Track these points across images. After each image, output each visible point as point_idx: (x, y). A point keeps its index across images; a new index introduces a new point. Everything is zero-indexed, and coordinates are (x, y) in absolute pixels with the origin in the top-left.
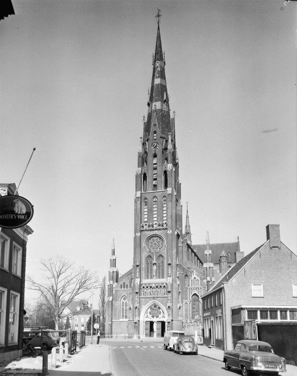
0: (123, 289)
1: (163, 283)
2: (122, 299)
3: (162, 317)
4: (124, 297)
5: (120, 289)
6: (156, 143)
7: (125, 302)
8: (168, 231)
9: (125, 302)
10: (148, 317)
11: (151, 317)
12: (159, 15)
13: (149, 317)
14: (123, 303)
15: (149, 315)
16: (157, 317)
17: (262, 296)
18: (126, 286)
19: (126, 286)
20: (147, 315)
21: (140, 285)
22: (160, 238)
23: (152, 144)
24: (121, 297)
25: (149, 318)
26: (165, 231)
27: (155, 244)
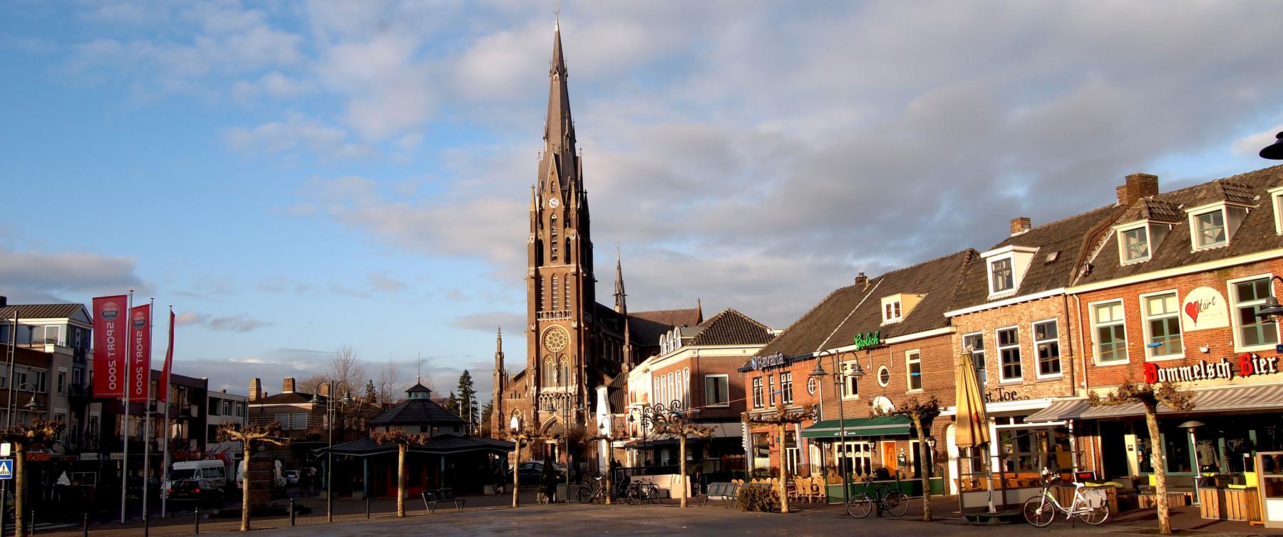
27: (556, 340)
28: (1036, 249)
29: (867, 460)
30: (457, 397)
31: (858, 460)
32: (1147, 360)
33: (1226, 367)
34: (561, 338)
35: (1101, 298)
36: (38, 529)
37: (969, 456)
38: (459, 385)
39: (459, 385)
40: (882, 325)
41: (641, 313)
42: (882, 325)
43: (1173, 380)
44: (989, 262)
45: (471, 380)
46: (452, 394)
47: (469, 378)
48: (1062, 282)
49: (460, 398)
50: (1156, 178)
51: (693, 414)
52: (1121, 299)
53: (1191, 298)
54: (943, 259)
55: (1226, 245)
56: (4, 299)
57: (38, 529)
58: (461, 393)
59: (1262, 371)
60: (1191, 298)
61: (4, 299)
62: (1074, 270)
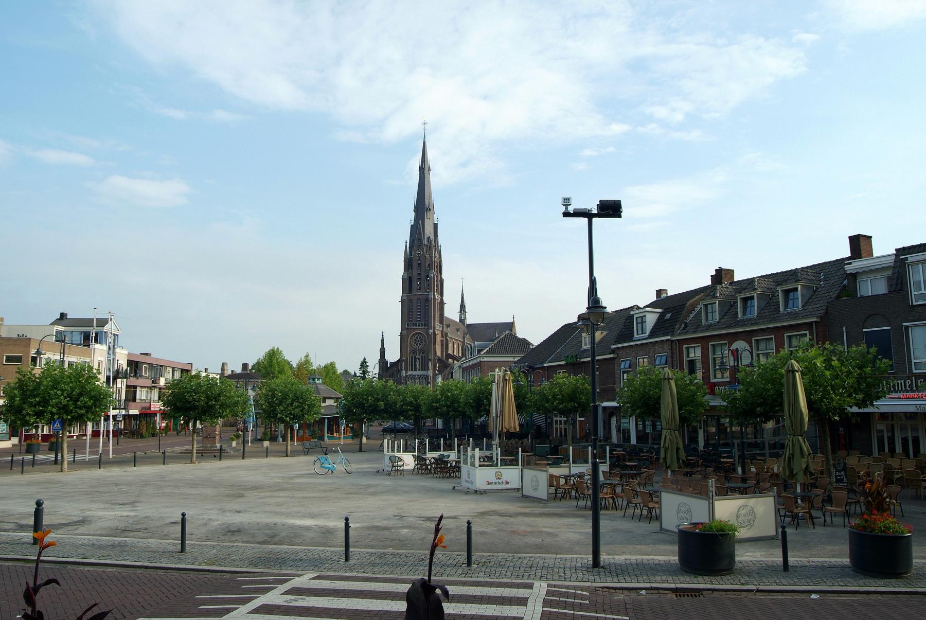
27: (419, 341)
28: (660, 311)
29: (565, 429)
30: (358, 375)
31: (561, 429)
32: (711, 381)
33: (901, 383)
35: (690, 343)
36: (903, 387)
37: (32, 457)
38: (360, 367)
39: (360, 367)
40: (582, 349)
41: (515, 329)
42: (582, 349)
43: (900, 389)
44: (635, 316)
45: (367, 364)
46: (355, 373)
47: (366, 362)
48: (126, 370)
49: (360, 375)
50: (716, 270)
51: (164, 410)
52: (700, 345)
53: (734, 347)
54: (621, 310)
55: (755, 317)
56: (2, 319)
57: (903, 387)
58: (361, 372)
59: (908, 388)
60: (734, 347)
61: (2, 319)
62: (678, 326)
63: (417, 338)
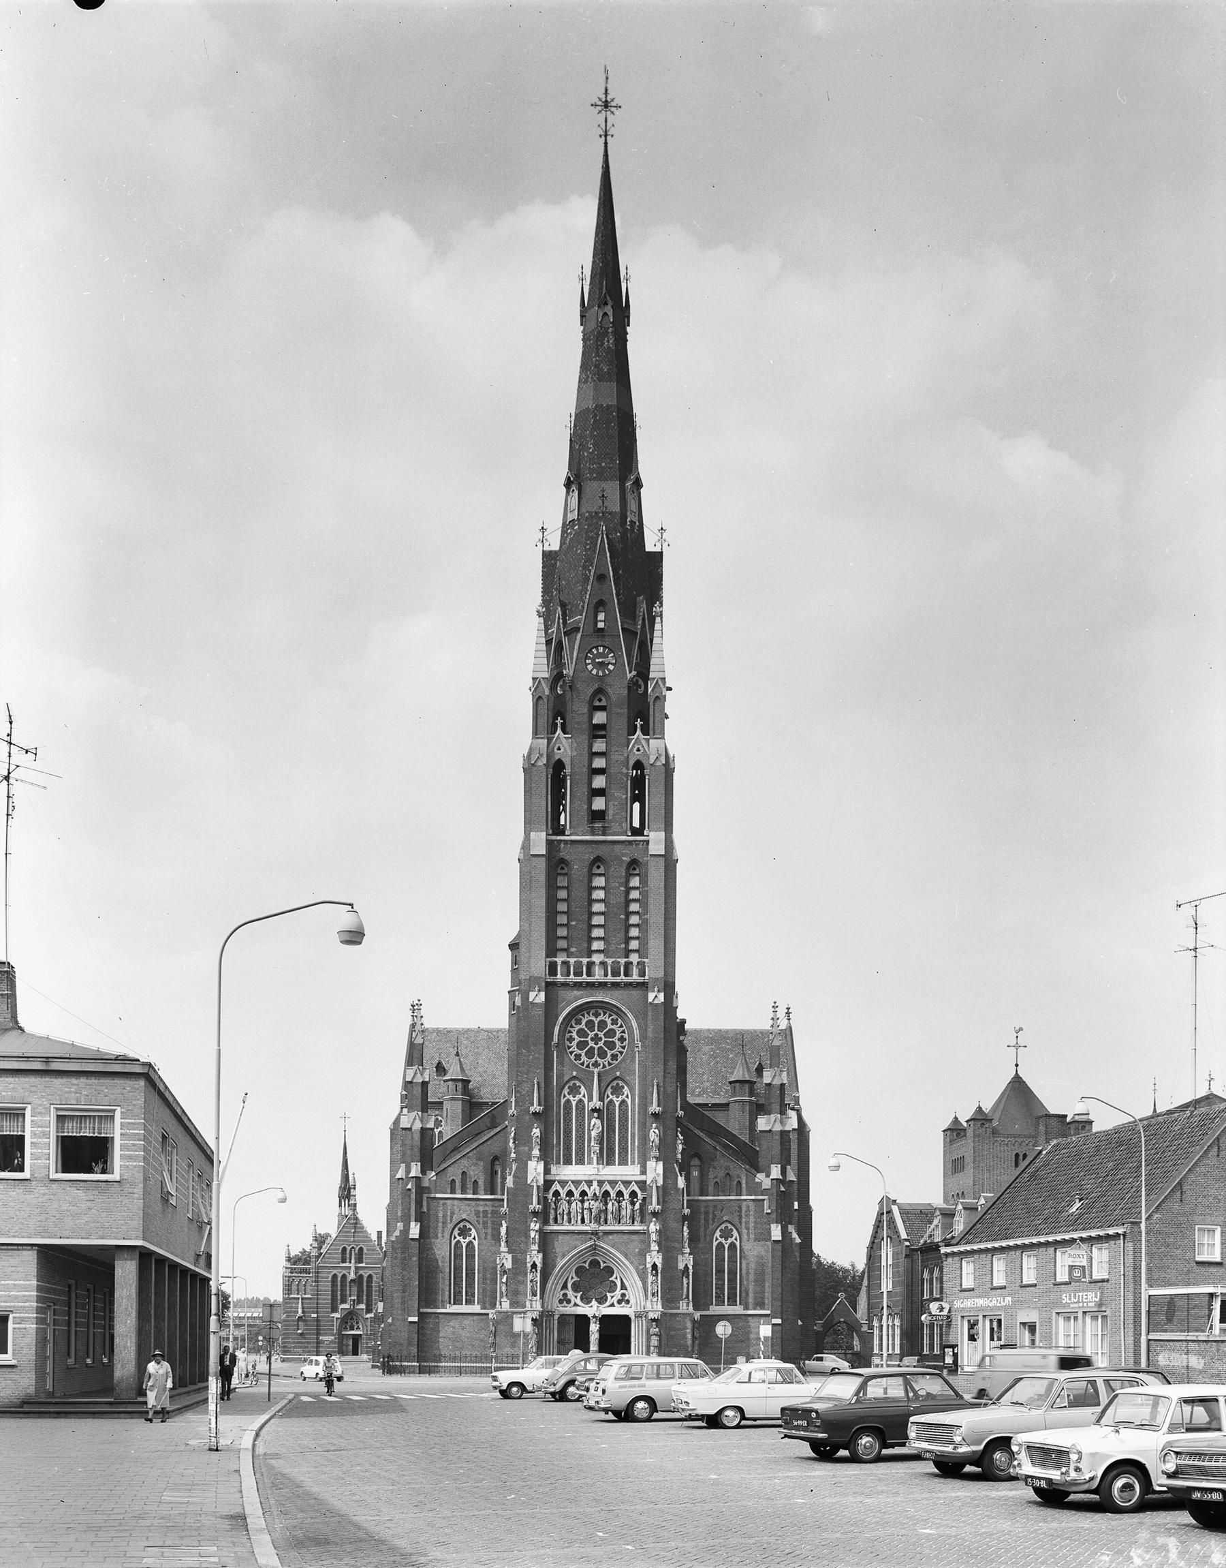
0: (640, 1355)
1: (627, 1183)
2: (456, 1232)
3: (619, 1302)
4: (461, 1225)
5: (341, 1265)
6: (589, 652)
7: (464, 1242)
8: (651, 996)
9: (464, 1242)
10: (569, 1301)
11: (578, 1301)
12: (606, 101)
13: (573, 1300)
14: (721, 1246)
15: (570, 1293)
16: (602, 1300)
17: (1218, 1259)
18: (470, 1186)
19: (470, 1186)
20: (565, 1295)
21: (548, 1184)
22: (619, 1012)
23: (590, 651)
24: (450, 1226)
25: (572, 1303)
26: (635, 993)
27: (596, 1039)
34: (611, 1045)
63: (590, 1024)
